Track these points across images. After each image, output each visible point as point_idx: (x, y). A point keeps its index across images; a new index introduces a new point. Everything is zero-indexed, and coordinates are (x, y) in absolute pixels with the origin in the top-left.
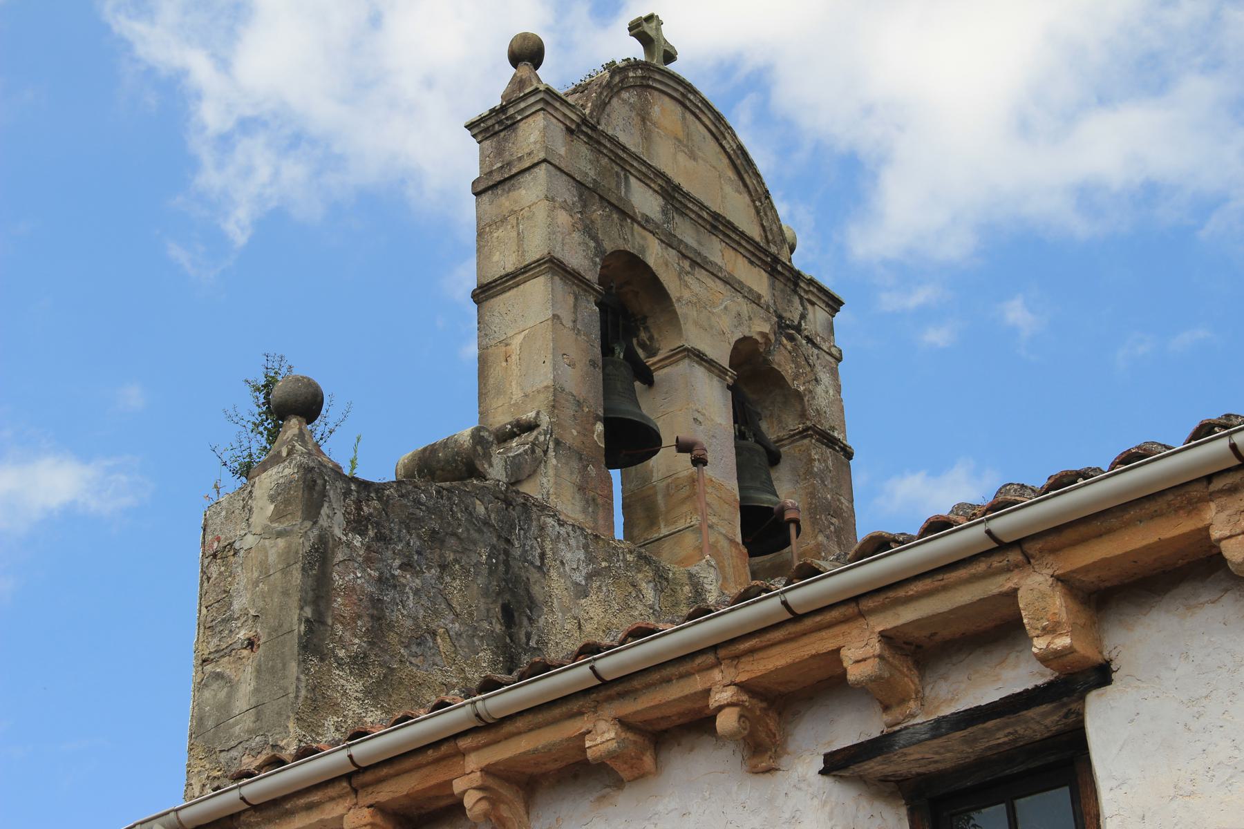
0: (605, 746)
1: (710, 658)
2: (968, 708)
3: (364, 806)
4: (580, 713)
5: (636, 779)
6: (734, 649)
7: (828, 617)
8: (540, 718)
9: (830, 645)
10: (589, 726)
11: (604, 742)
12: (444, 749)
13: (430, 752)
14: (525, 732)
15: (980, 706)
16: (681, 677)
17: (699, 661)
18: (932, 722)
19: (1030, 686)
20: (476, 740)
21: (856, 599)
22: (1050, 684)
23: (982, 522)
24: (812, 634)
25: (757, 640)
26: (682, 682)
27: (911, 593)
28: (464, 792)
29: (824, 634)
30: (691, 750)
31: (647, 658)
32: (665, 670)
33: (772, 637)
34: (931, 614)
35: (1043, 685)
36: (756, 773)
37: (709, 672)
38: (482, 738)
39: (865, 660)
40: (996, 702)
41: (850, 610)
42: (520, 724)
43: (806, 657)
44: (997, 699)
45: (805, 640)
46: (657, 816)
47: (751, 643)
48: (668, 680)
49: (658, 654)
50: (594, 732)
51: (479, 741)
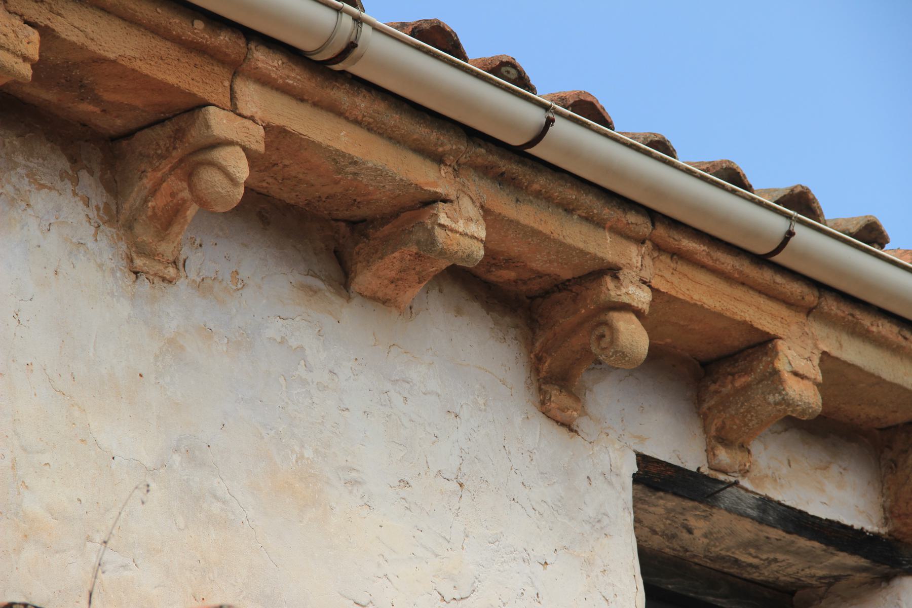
0: (466, 242)
1: (641, 225)
2: (686, 501)
3: (21, 16)
4: (438, 159)
5: (374, 298)
6: (676, 237)
7: (788, 287)
8: (394, 119)
9: (767, 324)
10: (452, 193)
11: (466, 234)
12: (223, 39)
13: (199, 25)
14: (347, 118)
15: (806, 513)
16: (588, 219)
17: (632, 218)
18: (757, 497)
19: (857, 525)
20: (286, 72)
21: (821, 287)
22: (876, 537)
23: (789, 217)
24: (751, 292)
25: (705, 248)
26: (586, 228)
27: (874, 329)
28: (230, 143)
29: (762, 301)
30: (459, 312)
31: (608, 168)
32: (587, 195)
33: (722, 260)
34: (872, 371)
35: (870, 533)
36: (549, 417)
37: (624, 241)
38: (295, 76)
39: (802, 378)
40: (820, 519)
41: (810, 296)
42: (363, 104)
43: (738, 318)
44: (824, 517)
45: (739, 292)
46: (407, 386)
47: (694, 245)
48: (568, 209)
49: (620, 173)
50: (455, 205)
51: (288, 77)
